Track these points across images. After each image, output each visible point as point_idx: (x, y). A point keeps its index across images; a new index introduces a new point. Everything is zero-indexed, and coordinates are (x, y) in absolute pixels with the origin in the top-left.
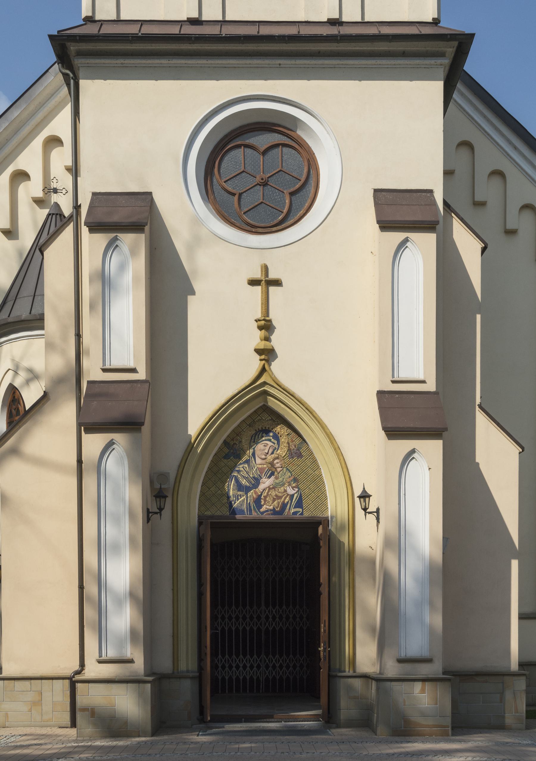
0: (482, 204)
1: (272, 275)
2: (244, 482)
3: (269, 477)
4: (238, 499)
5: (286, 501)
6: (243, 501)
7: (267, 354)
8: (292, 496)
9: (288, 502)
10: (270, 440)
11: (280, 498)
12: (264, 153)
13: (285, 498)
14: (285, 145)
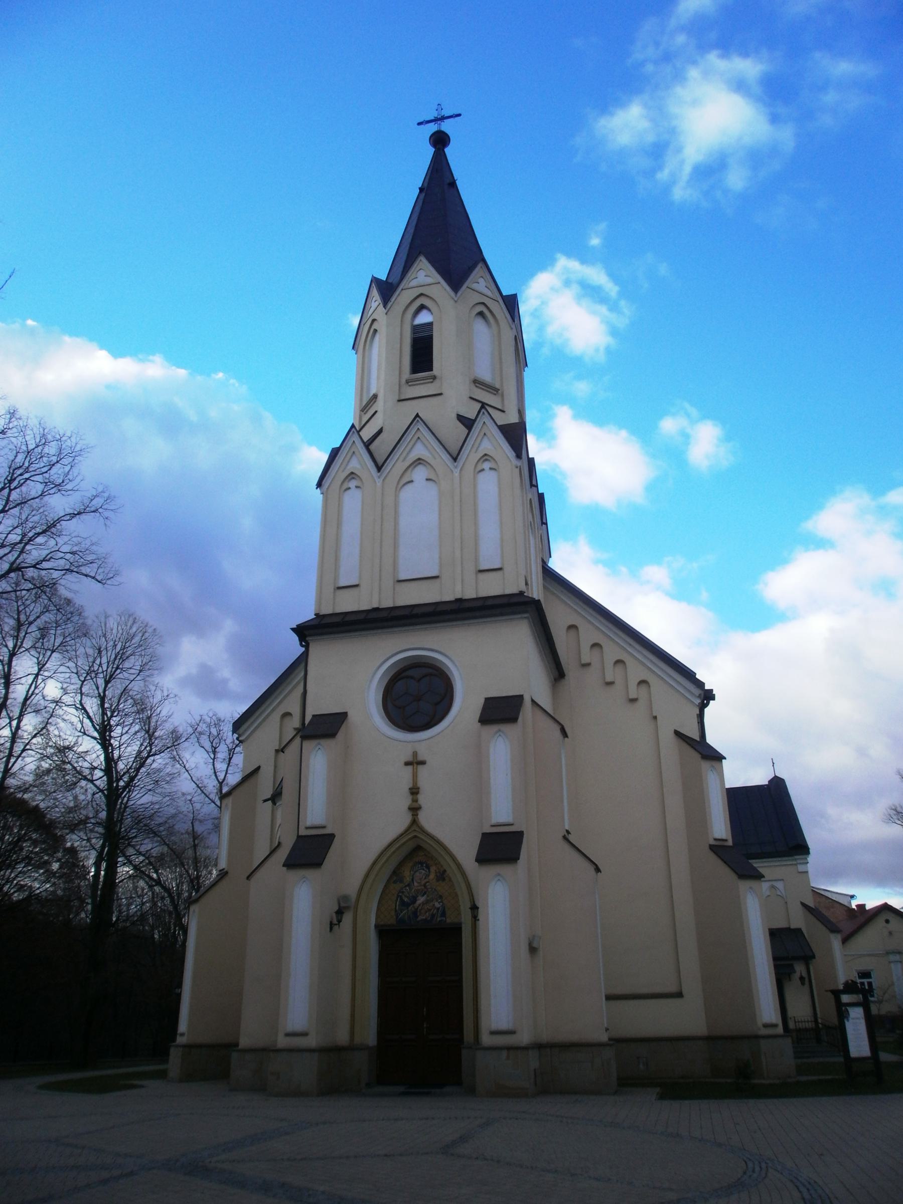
1: (420, 758)
7: (415, 809)
8: (438, 909)
11: (430, 910)
12: (419, 680)
14: (431, 675)
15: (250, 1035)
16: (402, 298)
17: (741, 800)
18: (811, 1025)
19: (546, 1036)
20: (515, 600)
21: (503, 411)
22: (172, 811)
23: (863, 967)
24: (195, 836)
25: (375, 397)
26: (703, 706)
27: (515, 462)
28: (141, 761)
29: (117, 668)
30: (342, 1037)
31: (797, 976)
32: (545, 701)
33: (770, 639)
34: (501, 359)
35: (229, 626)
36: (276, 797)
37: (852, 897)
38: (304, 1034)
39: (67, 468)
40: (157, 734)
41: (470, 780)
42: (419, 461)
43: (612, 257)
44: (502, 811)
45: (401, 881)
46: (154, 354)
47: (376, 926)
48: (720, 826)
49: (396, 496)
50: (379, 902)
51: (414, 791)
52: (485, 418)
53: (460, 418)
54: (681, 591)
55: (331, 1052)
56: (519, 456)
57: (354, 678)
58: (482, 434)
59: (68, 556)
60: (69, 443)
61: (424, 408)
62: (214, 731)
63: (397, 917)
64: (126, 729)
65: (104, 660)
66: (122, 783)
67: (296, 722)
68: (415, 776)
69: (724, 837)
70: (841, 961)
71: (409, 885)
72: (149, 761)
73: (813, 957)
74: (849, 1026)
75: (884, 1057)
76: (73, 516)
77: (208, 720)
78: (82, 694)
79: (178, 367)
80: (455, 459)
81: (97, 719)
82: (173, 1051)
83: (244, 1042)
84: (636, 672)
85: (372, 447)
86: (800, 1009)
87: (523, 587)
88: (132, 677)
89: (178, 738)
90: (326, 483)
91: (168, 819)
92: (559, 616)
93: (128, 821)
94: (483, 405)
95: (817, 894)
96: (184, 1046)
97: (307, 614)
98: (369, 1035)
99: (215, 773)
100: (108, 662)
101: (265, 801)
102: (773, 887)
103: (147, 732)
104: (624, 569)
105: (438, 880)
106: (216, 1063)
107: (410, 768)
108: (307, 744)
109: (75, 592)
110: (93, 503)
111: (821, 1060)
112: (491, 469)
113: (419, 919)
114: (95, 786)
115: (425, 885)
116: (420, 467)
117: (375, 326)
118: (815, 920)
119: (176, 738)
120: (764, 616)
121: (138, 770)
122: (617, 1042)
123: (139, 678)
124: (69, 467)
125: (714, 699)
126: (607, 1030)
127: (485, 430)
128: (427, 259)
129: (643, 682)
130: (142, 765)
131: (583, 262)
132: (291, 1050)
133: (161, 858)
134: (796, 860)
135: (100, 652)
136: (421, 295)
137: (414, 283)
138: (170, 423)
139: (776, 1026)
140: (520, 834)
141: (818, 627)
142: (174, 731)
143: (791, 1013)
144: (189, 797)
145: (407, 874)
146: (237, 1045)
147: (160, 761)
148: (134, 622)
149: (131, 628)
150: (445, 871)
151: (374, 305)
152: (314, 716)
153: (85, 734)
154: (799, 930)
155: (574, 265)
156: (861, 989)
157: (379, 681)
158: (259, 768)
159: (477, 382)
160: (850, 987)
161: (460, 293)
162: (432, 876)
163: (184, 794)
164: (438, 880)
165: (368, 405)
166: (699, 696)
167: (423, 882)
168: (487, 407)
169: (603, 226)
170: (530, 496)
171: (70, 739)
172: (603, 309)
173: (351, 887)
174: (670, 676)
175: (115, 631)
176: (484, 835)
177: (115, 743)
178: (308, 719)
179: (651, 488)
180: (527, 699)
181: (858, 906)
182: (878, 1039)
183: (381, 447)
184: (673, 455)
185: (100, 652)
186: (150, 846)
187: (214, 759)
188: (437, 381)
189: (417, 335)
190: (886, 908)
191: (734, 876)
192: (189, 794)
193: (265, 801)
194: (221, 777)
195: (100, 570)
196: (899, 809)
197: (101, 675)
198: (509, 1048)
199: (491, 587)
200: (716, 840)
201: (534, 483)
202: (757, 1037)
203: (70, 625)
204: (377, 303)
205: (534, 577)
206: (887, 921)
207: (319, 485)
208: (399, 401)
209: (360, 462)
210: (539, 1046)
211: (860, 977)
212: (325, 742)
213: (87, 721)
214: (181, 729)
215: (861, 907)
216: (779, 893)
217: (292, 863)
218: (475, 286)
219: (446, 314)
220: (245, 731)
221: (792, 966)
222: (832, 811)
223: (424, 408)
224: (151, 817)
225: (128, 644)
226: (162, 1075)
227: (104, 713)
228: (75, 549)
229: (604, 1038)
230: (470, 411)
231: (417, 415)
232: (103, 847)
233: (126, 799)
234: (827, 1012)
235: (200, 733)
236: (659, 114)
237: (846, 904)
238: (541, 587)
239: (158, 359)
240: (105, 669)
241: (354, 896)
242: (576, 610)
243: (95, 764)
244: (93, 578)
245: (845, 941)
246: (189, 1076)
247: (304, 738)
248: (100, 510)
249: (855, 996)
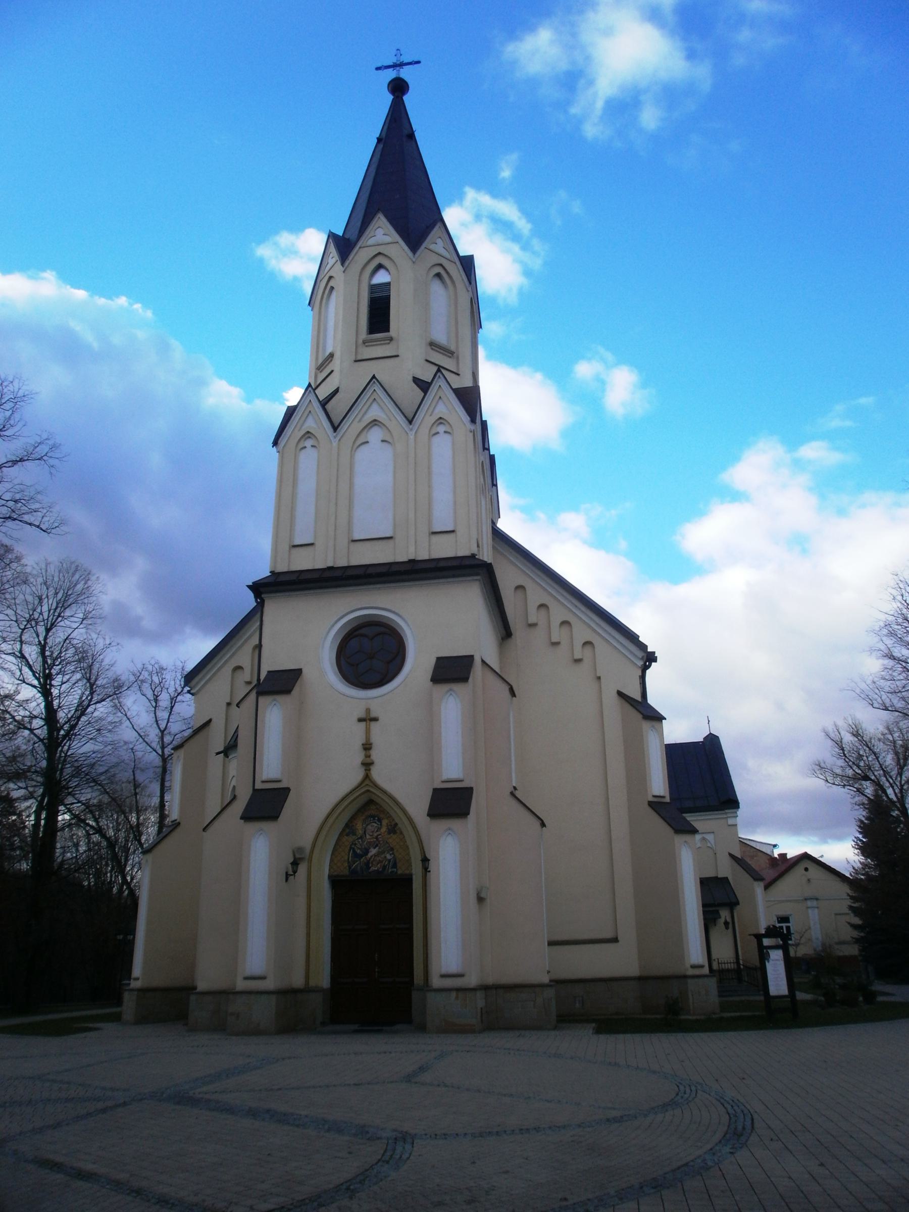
0: (556, 644)
1: (373, 715)
2: (358, 851)
7: (367, 765)
8: (389, 861)
15: (207, 978)
16: (360, 256)
17: (680, 756)
18: (732, 966)
19: (490, 981)
20: (467, 562)
21: (458, 375)
22: (115, 760)
23: (782, 913)
24: (136, 785)
25: (331, 356)
26: (645, 668)
27: (470, 426)
28: (82, 709)
29: (59, 616)
30: (298, 981)
31: (722, 920)
32: (494, 663)
33: (689, 591)
34: (456, 319)
35: (141, 563)
36: (230, 748)
37: (775, 846)
38: (263, 978)
39: (8, 414)
40: (99, 683)
41: (420, 736)
42: (375, 423)
43: (521, 191)
44: (452, 768)
45: (355, 835)
46: (44, 270)
47: (330, 877)
48: (658, 784)
49: (352, 457)
50: (333, 854)
51: (367, 747)
52: (440, 382)
53: (416, 380)
54: (600, 540)
55: (287, 994)
56: (473, 421)
57: (308, 635)
58: (437, 397)
59: (11, 504)
60: (11, 388)
61: (381, 370)
62: (156, 679)
63: (350, 867)
64: (67, 677)
65: (45, 608)
66: (62, 732)
67: (246, 675)
68: (368, 732)
69: (662, 794)
70: (762, 907)
71: (361, 838)
72: (90, 710)
73: (737, 903)
74: (769, 966)
75: (800, 996)
76: (15, 462)
77: (150, 668)
78: (22, 642)
79: (75, 288)
80: (410, 422)
81: (38, 667)
82: (126, 996)
83: (202, 986)
84: (581, 633)
85: (329, 407)
86: (724, 952)
87: (474, 550)
88: (75, 625)
89: (120, 687)
90: (282, 442)
91: (111, 767)
92: (508, 576)
93: (68, 770)
94: (440, 369)
95: (744, 844)
96: (140, 990)
97: (263, 572)
98: (323, 979)
99: (157, 721)
100: (49, 611)
101: (218, 754)
102: (704, 839)
103: (89, 680)
104: (542, 515)
105: (389, 833)
106: (173, 1005)
107: (363, 724)
108: (262, 700)
109: (17, 540)
110: (38, 449)
111: (743, 998)
112: (445, 432)
113: (371, 870)
114: (35, 735)
115: (377, 838)
116: (375, 429)
117: (331, 284)
118: (738, 867)
119: (117, 688)
120: (683, 568)
121: (79, 718)
122: (557, 983)
123: (81, 626)
124: (10, 412)
125: (656, 661)
126: (548, 972)
127: (440, 394)
128: (386, 216)
129: (587, 643)
130: (83, 713)
131: (495, 195)
132: (250, 993)
133: (100, 806)
134: (726, 813)
135: (40, 599)
136: (380, 253)
137: (371, 242)
138: (67, 348)
139: (702, 967)
140: (469, 790)
141: (733, 583)
142: (116, 680)
143: (714, 955)
144: (131, 746)
145: (359, 826)
146: (195, 988)
147: (101, 710)
148: (76, 570)
149: (73, 575)
150: (396, 824)
151: (331, 262)
152: (269, 672)
153: (24, 682)
154: (726, 879)
155: (486, 200)
156: (780, 933)
158: (210, 720)
159: (433, 345)
160: (772, 932)
161: (418, 253)
162: (384, 829)
163: (126, 743)
164: (389, 833)
165: (323, 364)
166: (642, 659)
167: (375, 835)
168: (443, 371)
169: (514, 157)
170: (482, 458)
171: (9, 686)
172: (516, 248)
173: (306, 839)
174: (624, 646)
175: (56, 579)
176: (435, 790)
177: (55, 692)
178: (263, 676)
179: (567, 434)
180: (477, 661)
181: (780, 855)
182: (796, 980)
183: (338, 406)
184: (588, 400)
185: (40, 599)
186: (89, 796)
187: (155, 708)
188: (393, 342)
189: (376, 295)
190: (806, 857)
191: (668, 831)
192: (131, 743)
193: (218, 754)
194: (163, 726)
195: (45, 519)
196: (822, 765)
197: (42, 623)
198: (458, 990)
199: (444, 549)
200: (654, 796)
201: (486, 446)
202: (685, 977)
203: (8, 573)
204: (334, 260)
205: (485, 537)
206: (806, 869)
207: (275, 443)
208: (356, 361)
209: (316, 422)
210: (485, 988)
211: (779, 922)
212: (281, 698)
213: (26, 670)
214: (123, 678)
215: (783, 856)
216: (709, 845)
217: (249, 816)
218: (432, 247)
219: (403, 275)
220: (197, 683)
221: (717, 912)
222: (751, 763)
223: (381, 370)
224: (92, 766)
225: (70, 593)
226: (116, 1018)
227: (45, 661)
228: (18, 497)
229: (546, 980)
230: (427, 374)
231: (374, 377)
232: (43, 796)
233: (66, 748)
234: (750, 955)
235: (143, 681)
236: (571, 40)
237: (769, 853)
238: (490, 548)
239: (49, 275)
240: (46, 617)
241: (308, 847)
242: (523, 571)
243: (35, 713)
244: (38, 527)
245: (767, 887)
246: (144, 1018)
247: (259, 694)
248: (45, 458)
249: (774, 940)
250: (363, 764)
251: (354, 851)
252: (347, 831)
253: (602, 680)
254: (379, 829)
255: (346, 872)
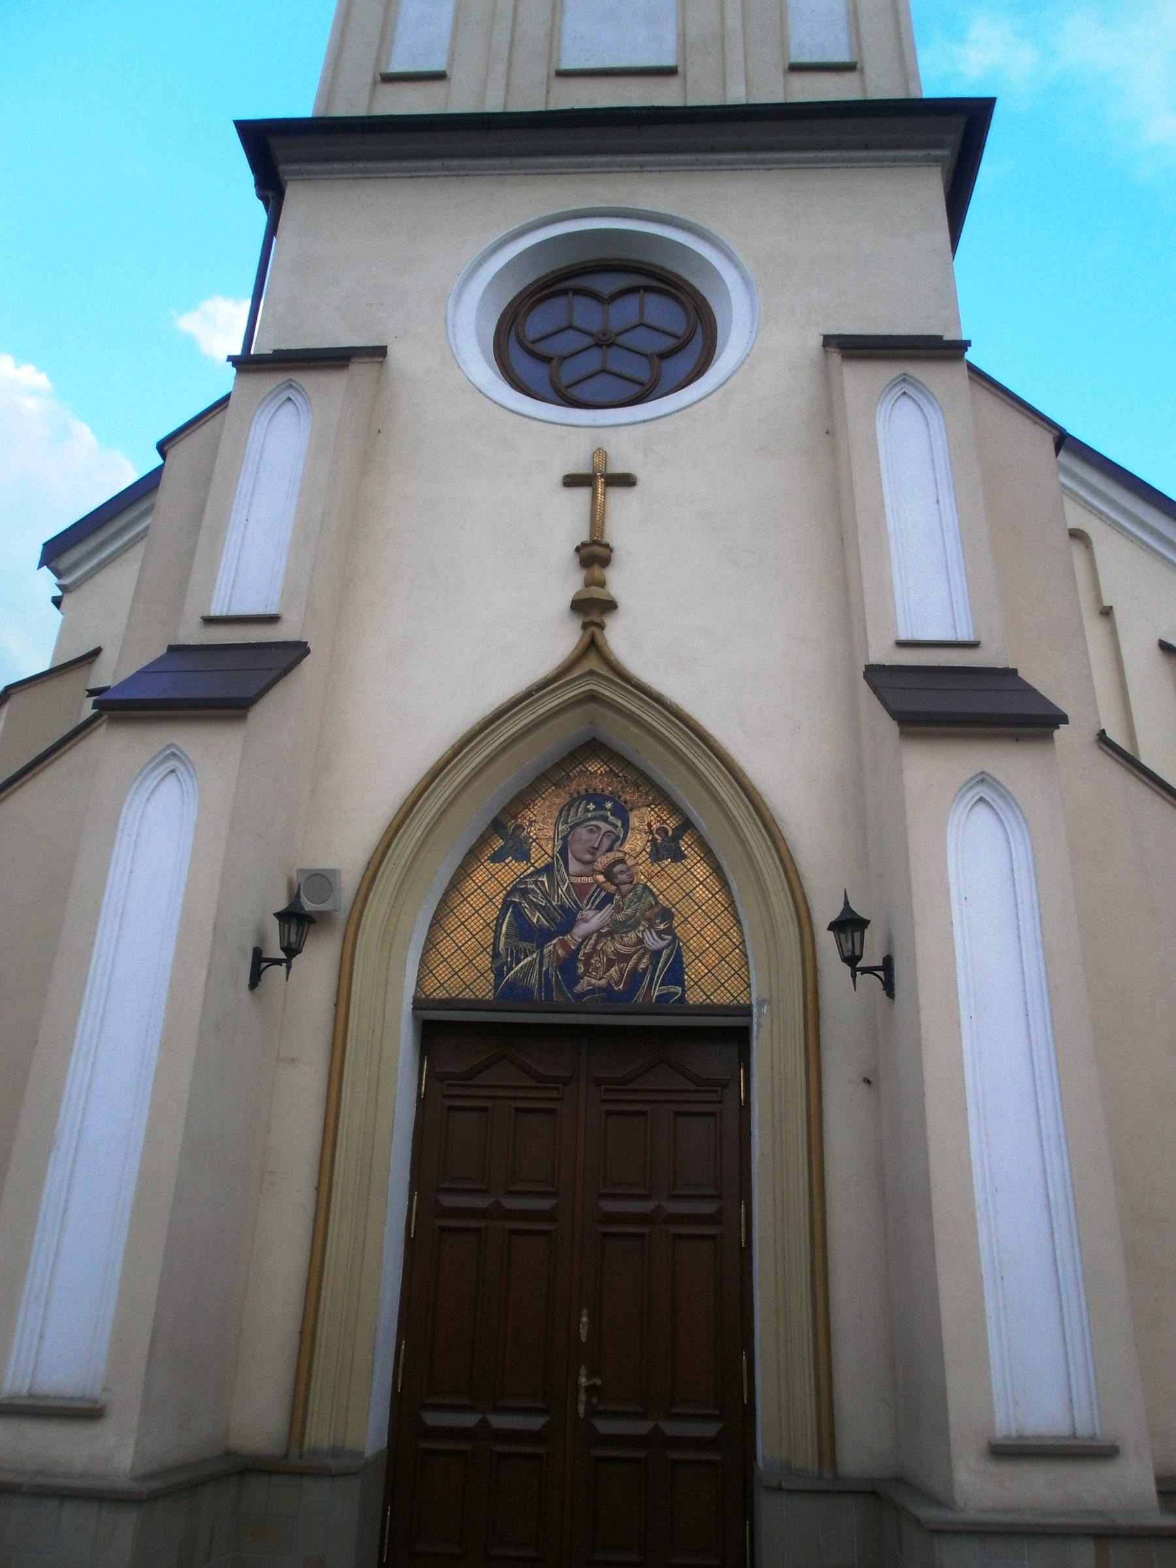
1: (617, 468)
2: (536, 918)
3: (600, 907)
4: (518, 961)
5: (642, 966)
6: (531, 965)
7: (593, 608)
8: (657, 954)
9: (645, 970)
10: (605, 819)
11: (626, 958)
13: (639, 960)
38: (86, 1413)
47: (419, 1004)
50: (423, 962)
51: (594, 555)
63: (499, 974)
68: (597, 519)
71: (548, 869)
105: (657, 855)
107: (582, 495)
113: (583, 986)
115: (608, 873)
145: (542, 827)
157: (495, 277)
158: (97, 652)
162: (636, 842)
164: (657, 855)
167: (603, 861)
173: (346, 848)
220: (76, 565)
241: (349, 883)
250: (579, 606)
251: (518, 914)
252: (498, 843)
253: (1118, 613)
254: (616, 841)
255: (484, 990)
